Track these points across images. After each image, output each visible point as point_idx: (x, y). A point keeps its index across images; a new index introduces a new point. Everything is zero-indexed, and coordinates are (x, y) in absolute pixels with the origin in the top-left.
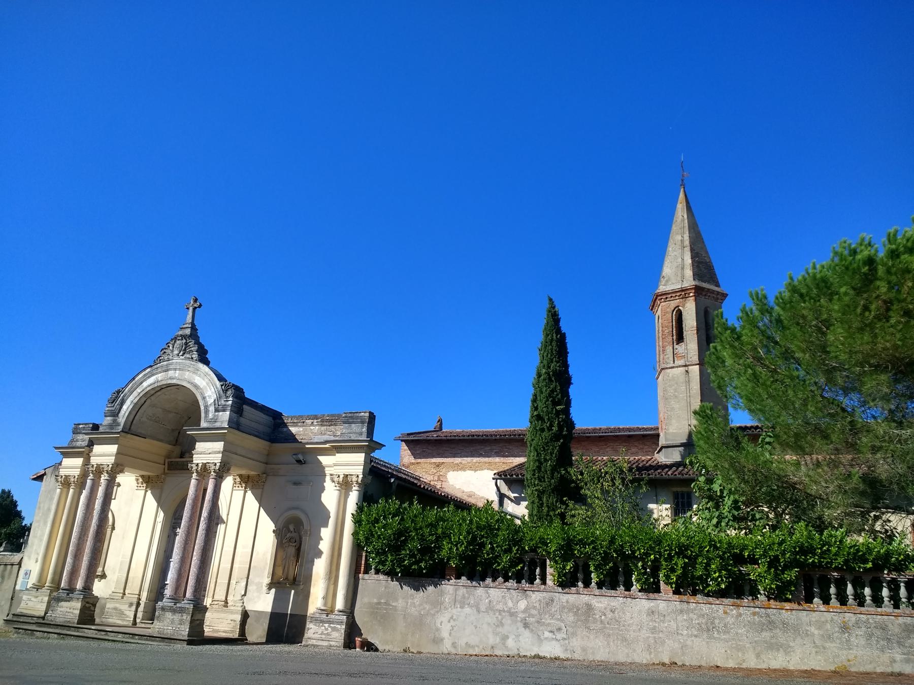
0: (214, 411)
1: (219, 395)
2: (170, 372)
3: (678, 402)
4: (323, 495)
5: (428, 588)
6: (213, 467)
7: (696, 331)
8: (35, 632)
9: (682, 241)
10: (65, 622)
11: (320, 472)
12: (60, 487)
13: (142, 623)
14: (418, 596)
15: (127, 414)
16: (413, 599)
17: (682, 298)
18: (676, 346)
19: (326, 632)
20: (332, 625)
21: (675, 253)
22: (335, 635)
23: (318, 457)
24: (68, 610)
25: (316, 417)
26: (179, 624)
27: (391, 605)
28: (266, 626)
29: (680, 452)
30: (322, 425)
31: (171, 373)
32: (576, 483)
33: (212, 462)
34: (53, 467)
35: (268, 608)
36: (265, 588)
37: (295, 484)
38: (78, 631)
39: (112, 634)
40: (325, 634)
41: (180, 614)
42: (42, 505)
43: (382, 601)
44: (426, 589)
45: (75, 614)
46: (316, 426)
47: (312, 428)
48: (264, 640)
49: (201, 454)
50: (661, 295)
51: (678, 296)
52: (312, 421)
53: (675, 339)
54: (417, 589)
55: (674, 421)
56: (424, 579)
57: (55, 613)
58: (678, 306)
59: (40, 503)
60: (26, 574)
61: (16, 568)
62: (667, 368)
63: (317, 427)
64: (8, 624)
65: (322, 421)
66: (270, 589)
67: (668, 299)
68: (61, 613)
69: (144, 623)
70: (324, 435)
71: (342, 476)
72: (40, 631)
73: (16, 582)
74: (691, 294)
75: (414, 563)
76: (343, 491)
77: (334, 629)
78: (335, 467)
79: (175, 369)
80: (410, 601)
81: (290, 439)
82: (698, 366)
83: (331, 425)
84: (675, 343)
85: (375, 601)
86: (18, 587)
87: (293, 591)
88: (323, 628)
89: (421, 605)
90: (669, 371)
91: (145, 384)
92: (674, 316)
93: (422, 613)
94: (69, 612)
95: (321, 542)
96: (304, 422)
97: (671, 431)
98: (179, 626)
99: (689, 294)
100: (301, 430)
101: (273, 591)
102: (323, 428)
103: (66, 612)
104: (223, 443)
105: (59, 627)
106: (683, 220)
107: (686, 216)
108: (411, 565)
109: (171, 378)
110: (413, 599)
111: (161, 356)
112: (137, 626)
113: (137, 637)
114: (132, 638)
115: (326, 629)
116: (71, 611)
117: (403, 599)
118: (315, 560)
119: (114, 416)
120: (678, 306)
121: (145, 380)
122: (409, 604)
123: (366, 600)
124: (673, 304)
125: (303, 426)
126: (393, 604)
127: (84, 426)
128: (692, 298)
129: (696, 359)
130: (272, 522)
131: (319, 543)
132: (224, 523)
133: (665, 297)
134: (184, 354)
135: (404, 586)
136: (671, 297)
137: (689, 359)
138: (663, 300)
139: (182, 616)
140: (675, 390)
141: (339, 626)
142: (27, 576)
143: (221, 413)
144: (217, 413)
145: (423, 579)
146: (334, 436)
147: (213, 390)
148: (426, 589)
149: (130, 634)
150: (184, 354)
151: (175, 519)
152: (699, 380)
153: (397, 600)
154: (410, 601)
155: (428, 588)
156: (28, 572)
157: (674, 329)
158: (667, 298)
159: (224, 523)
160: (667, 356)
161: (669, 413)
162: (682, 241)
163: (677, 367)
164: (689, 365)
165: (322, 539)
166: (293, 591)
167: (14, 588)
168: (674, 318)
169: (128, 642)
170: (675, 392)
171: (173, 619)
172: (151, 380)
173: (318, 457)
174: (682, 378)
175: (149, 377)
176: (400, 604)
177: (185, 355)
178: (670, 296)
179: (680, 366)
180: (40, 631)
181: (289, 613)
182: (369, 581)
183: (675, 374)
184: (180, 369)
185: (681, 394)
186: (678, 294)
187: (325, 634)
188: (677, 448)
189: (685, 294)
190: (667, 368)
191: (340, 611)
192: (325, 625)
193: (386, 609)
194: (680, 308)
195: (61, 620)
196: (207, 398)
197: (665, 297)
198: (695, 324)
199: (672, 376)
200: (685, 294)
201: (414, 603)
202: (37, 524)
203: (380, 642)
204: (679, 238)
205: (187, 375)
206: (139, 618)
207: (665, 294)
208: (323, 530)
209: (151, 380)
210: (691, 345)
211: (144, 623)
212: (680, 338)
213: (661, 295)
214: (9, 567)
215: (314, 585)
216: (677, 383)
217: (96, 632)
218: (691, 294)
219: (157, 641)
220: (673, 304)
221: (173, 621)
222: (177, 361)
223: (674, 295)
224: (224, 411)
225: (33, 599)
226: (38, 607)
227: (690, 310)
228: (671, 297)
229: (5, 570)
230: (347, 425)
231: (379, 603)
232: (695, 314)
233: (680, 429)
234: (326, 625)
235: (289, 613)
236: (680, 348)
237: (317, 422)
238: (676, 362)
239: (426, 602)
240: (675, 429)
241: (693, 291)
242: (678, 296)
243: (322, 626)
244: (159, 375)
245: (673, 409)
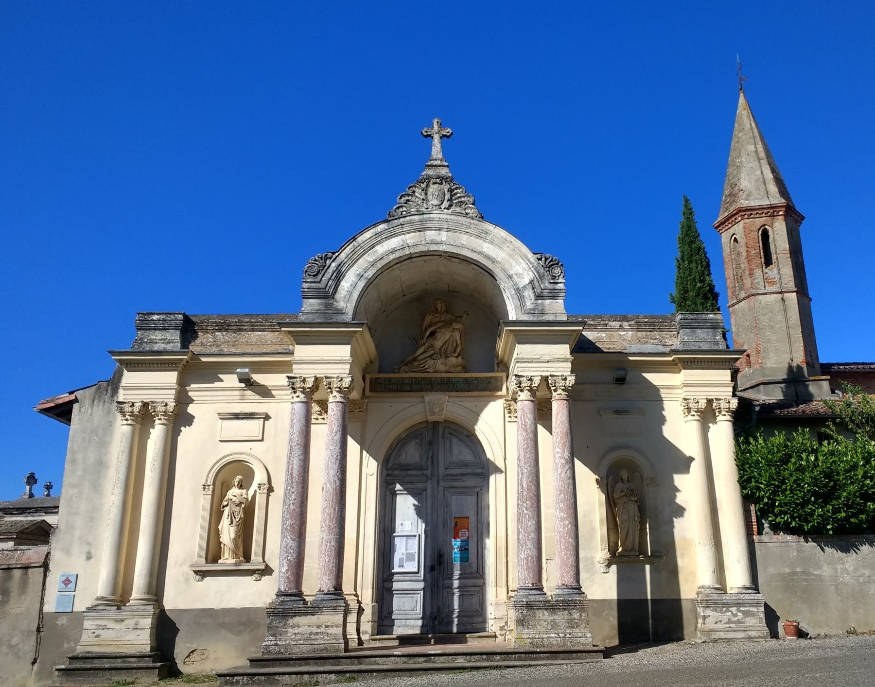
0: (533, 297)
1: (538, 273)
2: (428, 233)
3: (774, 333)
4: (664, 428)
5: (861, 548)
6: (562, 383)
7: (789, 255)
8: (277, 677)
9: (756, 152)
10: (314, 651)
11: (654, 396)
12: (130, 422)
13: (373, 640)
14: (849, 559)
15: (355, 295)
16: (843, 564)
17: (769, 216)
18: (766, 270)
19: (735, 619)
20: (741, 609)
21: (750, 164)
22: (750, 622)
23: (644, 375)
24: (315, 630)
25: (624, 319)
26: (569, 627)
27: (813, 575)
28: (614, 621)
29: (782, 388)
30: (638, 330)
31: (431, 235)
32: (841, 418)
33: (560, 374)
34: (93, 389)
35: (612, 594)
36: (601, 568)
37: (618, 412)
38: (361, 664)
39: (442, 659)
40: (734, 622)
41: (566, 612)
42: (79, 456)
43: (798, 570)
44: (859, 549)
45: (335, 635)
46: (628, 330)
47: (622, 333)
48: (616, 642)
49: (532, 362)
50: (744, 211)
51: (765, 214)
52: (620, 323)
53: (763, 262)
54: (845, 550)
55: (772, 355)
56: (854, 536)
57: (284, 638)
58: (764, 225)
59: (73, 453)
60: (67, 582)
61: (36, 575)
62: (758, 294)
63: (630, 333)
64: (68, 675)
65: (638, 324)
66: (609, 566)
67: (752, 216)
68: (299, 637)
69: (380, 639)
70: (646, 343)
71: (138, 405)
72: (290, 674)
73: (42, 599)
74: (781, 213)
75: (854, 515)
76: (138, 426)
77: (747, 614)
78: (685, 389)
79: (440, 229)
80: (839, 567)
81: (590, 349)
82: (795, 294)
83: (654, 330)
84: (764, 267)
85: (787, 570)
86: (48, 608)
87: (648, 567)
88: (730, 614)
89: (856, 570)
90: (760, 297)
91: (381, 249)
92: (760, 236)
93: (861, 581)
94: (317, 634)
95: (677, 494)
96: (606, 325)
97: (769, 365)
98: (568, 631)
99: (778, 212)
100: (603, 335)
101: (614, 568)
102: (640, 334)
103: (311, 633)
104: (176, 373)
105: (312, 661)
106: (752, 129)
107: (753, 125)
108: (847, 518)
109: (433, 242)
110: (843, 564)
111: (402, 207)
112: (365, 646)
113: (498, 657)
114: (487, 660)
115: (735, 615)
116: (323, 629)
117: (829, 564)
118: (675, 519)
119: (326, 297)
120: (764, 225)
121: (379, 242)
122: (839, 571)
123: (771, 570)
124: (759, 222)
125: (605, 330)
126: (816, 573)
127: (162, 317)
128: (781, 217)
129: (791, 285)
130: (587, 469)
131: (675, 496)
132: (502, 472)
133: (749, 213)
134: (451, 206)
135: (826, 548)
136: (757, 213)
137: (783, 285)
138: (746, 216)
139: (571, 614)
140: (770, 320)
141: (755, 609)
142: (71, 586)
143: (547, 302)
144: (540, 301)
145: (851, 536)
146: (664, 345)
147: (524, 265)
148: (859, 549)
149: (481, 654)
150: (451, 206)
151: (387, 470)
152: (797, 309)
153: (820, 568)
154: (839, 567)
155: (861, 548)
156: (73, 579)
157: (762, 251)
158: (751, 214)
159: (502, 472)
160: (756, 281)
161: (765, 345)
162: (756, 152)
163: (771, 293)
164: (785, 292)
165: (678, 490)
166: (648, 567)
167: (41, 610)
168: (760, 238)
169: (512, 667)
170: (770, 321)
171: (554, 621)
172: (394, 243)
173: (644, 375)
174: (779, 306)
175: (387, 238)
176: (826, 571)
177: (452, 209)
178: (755, 212)
179: (774, 293)
180: (290, 674)
181: (649, 597)
182: (771, 545)
183: (768, 302)
184: (448, 230)
185: (778, 324)
186: (765, 211)
187: (734, 622)
188: (780, 385)
189: (774, 212)
190: (758, 294)
191: (748, 588)
192: (731, 609)
193: (806, 580)
194: (767, 227)
195: (305, 648)
196: (514, 276)
197: (749, 213)
198: (788, 246)
199: (765, 304)
200: (774, 212)
201: (846, 569)
202: (75, 491)
203: (809, 625)
204: (752, 148)
205: (464, 239)
206: (366, 633)
207: (750, 210)
208: (679, 480)
209: (394, 243)
210: (783, 270)
211: (380, 639)
212: (768, 262)
213: (744, 211)
214: (17, 574)
215: (683, 555)
216: (771, 312)
217: (404, 659)
218: (781, 213)
219: (543, 659)
220: (759, 222)
221: (554, 625)
222: (439, 216)
223: (760, 212)
224: (554, 297)
225: (111, 625)
226: (128, 638)
227: (779, 231)
228: (757, 213)
229: (8, 578)
230: (688, 330)
231: (794, 573)
232: (786, 236)
233: (781, 363)
234: (734, 609)
235: (649, 597)
236: (772, 272)
237: (630, 325)
238: (767, 287)
239: (863, 566)
240: (774, 364)
241: (784, 209)
242: (765, 214)
243: (727, 611)
244: (407, 236)
245: (769, 341)
